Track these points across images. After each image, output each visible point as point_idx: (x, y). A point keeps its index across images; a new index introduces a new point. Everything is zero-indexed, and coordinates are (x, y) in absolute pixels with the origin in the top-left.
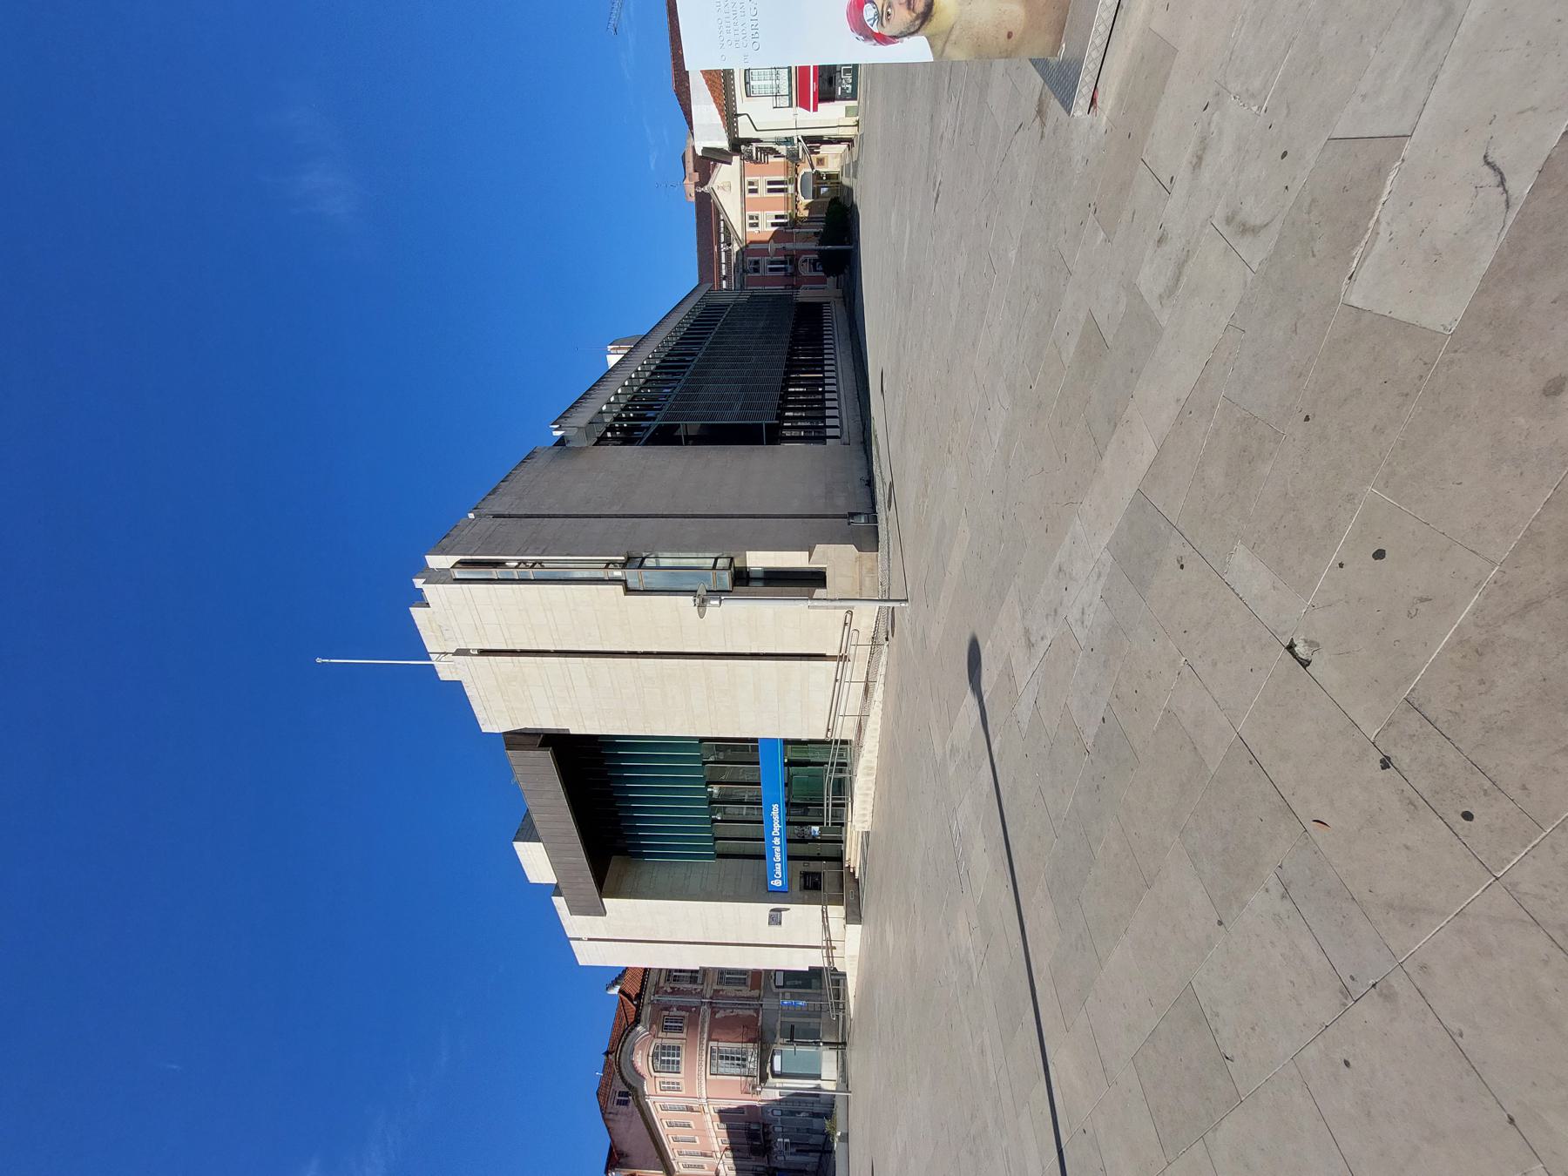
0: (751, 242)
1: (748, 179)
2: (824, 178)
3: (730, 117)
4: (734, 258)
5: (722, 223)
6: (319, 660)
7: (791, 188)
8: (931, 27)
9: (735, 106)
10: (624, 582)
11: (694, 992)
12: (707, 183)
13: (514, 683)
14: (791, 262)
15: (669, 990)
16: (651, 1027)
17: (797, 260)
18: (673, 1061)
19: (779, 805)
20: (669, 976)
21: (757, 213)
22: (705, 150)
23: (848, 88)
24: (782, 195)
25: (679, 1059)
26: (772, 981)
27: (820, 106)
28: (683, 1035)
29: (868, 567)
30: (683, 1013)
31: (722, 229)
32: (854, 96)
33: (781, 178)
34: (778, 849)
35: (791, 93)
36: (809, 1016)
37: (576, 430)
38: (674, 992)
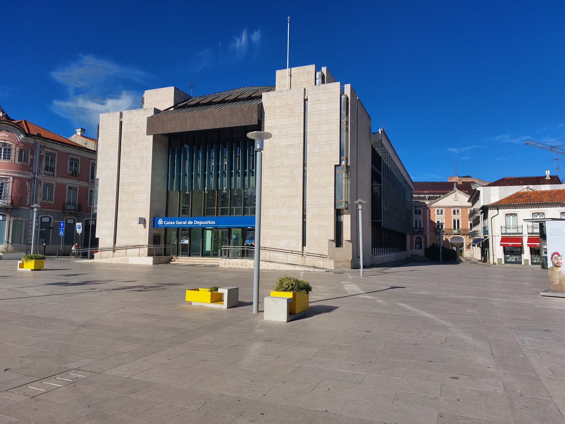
0: (430, 210)
1: (460, 209)
2: (461, 249)
3: (497, 206)
4: (422, 201)
5: (439, 196)
6: (289, 18)
7: (456, 232)
8: (554, 267)
9: (501, 209)
10: (340, 165)
11: (40, 169)
12: (458, 189)
13: (289, 112)
14: (419, 231)
15: (42, 154)
16: (22, 143)
17: (421, 234)
18: (4, 155)
19: (214, 225)
20: (49, 154)
21: (444, 214)
22: (479, 192)
23: (509, 259)
24: (453, 227)
25: (2, 158)
26: (44, 215)
27: (502, 247)
28: (17, 162)
29: (345, 265)
30: (29, 162)
31: (436, 196)
32: (506, 262)
33: (460, 227)
34: (185, 223)
35: (507, 234)
36: (25, 237)
37: (380, 139)
38: (41, 157)
